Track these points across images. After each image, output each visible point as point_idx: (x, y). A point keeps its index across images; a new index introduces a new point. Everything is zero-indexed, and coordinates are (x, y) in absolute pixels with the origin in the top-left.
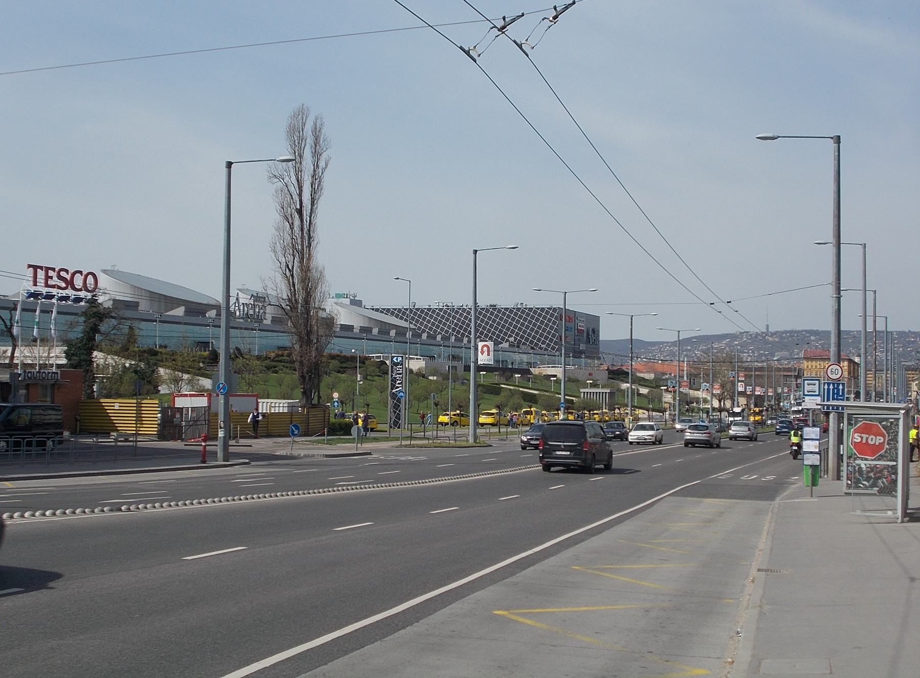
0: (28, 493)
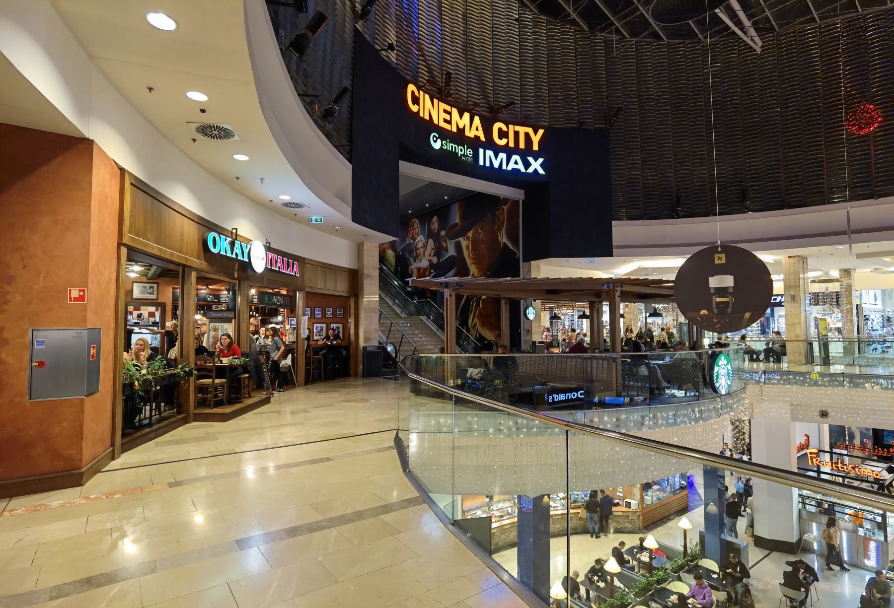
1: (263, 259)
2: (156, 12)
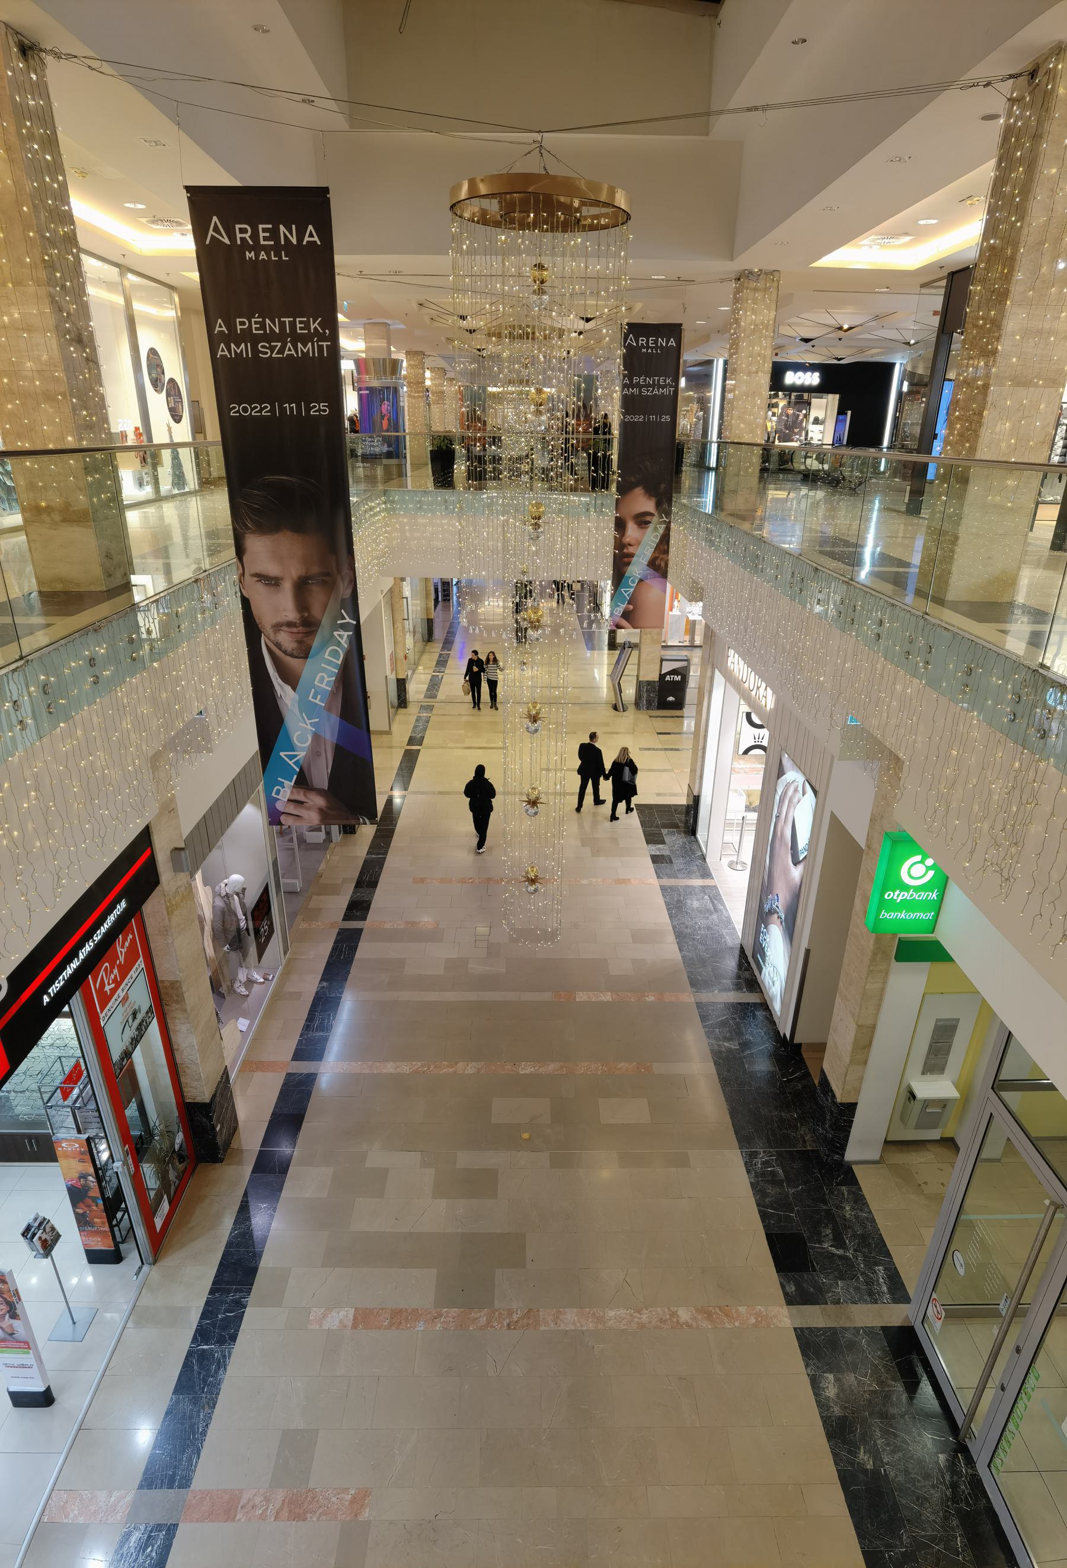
1: (135, 1014)
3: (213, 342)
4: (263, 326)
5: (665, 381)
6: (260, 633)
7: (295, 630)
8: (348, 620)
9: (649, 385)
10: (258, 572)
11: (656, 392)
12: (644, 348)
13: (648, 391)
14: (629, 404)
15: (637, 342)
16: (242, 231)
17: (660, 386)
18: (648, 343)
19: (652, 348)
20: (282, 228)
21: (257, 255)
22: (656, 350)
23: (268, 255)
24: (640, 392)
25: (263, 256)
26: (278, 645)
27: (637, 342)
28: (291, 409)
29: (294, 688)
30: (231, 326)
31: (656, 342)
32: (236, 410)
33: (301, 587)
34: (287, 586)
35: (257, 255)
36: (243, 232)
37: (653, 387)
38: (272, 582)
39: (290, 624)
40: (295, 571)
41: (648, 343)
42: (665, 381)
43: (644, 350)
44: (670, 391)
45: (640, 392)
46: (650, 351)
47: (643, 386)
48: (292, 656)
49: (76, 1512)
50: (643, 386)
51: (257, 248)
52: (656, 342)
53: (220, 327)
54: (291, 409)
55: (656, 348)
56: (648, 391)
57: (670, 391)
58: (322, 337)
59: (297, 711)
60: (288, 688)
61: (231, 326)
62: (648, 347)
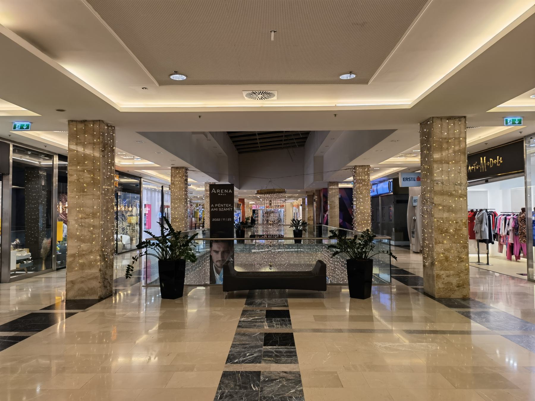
0: (511, 173)
1: (310, 135)
2: (421, 277)
3: (211, 208)
4: (220, 205)
5: (228, 205)
6: (213, 263)
7: (220, 262)
8: (232, 260)
9: (222, 207)
10: (214, 250)
11: (225, 209)
12: (219, 193)
13: (221, 209)
14: (213, 215)
15: (216, 191)
16: (218, 191)
17: (226, 207)
18: (220, 191)
19: (222, 193)
20: (225, 190)
21: (220, 194)
22: (224, 194)
23: (222, 194)
24: (218, 210)
25: (221, 194)
26: (217, 265)
27: (216, 191)
28: (224, 220)
29: (219, 275)
30: (214, 205)
31: (224, 191)
32: (213, 220)
33: (223, 253)
34: (220, 253)
35: (220, 194)
36: (218, 191)
37: (222, 208)
38: (217, 252)
39: (219, 261)
40: (222, 249)
41: (220, 191)
42: (228, 205)
43: (219, 194)
44: (230, 209)
45: (218, 210)
46: (221, 194)
47: (219, 207)
48: (219, 268)
49: (320, 255)
50: (219, 207)
51: (220, 193)
52: (224, 191)
53: (212, 206)
54: (224, 220)
55: (224, 193)
56: (221, 209)
57: (230, 209)
58: (231, 207)
59: (219, 280)
60: (218, 275)
61: (214, 205)
62: (220, 193)
